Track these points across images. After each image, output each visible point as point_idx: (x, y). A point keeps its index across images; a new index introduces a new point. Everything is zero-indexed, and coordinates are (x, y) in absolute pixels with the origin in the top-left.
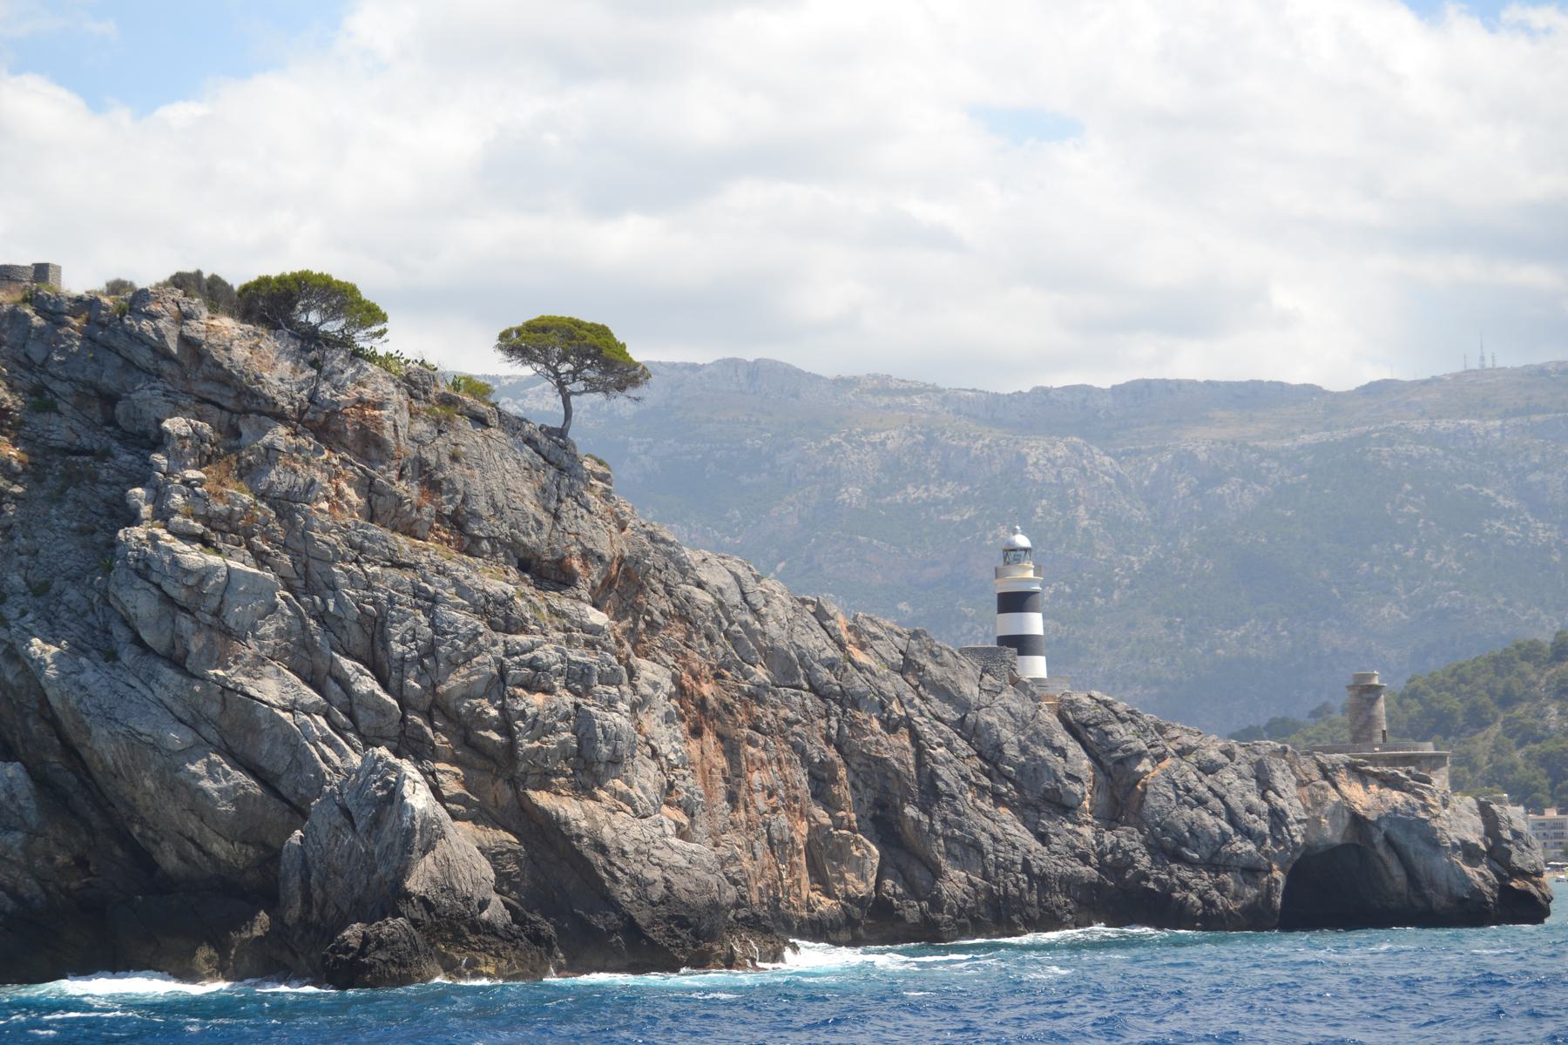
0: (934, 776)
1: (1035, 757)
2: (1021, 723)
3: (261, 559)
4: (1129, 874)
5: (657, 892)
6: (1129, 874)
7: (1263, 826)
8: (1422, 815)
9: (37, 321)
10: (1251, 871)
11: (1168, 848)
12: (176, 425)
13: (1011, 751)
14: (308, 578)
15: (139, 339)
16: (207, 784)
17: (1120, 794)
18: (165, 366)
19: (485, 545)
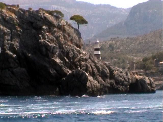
0: (94, 72)
1: (103, 71)
2: (102, 66)
3: (55, 44)
4: (113, 86)
5: (96, 86)
6: (113, 86)
7: (127, 80)
8: (144, 79)
9: (22, 13)
10: (126, 86)
11: (118, 82)
12: (44, 27)
13: (101, 70)
14: (61, 47)
15: (39, 16)
16: (51, 72)
17: (112, 76)
18: (42, 20)
19: (74, 43)
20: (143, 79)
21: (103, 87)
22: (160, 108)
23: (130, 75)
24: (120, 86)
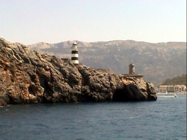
6: (86, 93)
10: (107, 92)
13: (68, 74)
20: (133, 83)
21: (68, 94)
22: (184, 122)
23: (116, 80)
24: (95, 93)
